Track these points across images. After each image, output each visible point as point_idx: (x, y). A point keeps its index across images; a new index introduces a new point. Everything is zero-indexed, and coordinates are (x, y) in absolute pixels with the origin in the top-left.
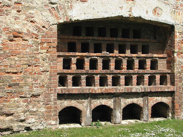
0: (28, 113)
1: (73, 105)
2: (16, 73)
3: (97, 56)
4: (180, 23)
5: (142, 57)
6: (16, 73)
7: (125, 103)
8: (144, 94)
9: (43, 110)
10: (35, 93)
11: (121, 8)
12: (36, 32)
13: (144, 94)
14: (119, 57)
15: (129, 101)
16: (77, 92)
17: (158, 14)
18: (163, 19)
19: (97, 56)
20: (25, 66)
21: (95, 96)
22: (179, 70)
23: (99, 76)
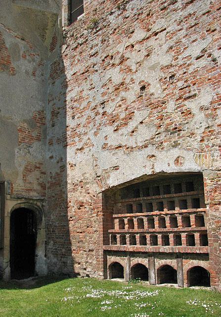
0: (88, 264)
1: (117, 261)
2: (81, 233)
3: (143, 216)
4: (209, 168)
5: (184, 213)
6: (81, 233)
7: (159, 263)
8: (179, 256)
9: (95, 262)
10: (91, 248)
11: (145, 167)
12: (90, 201)
13: (179, 256)
14: (162, 215)
15: (163, 262)
16: (116, 250)
17: (181, 163)
18: (187, 168)
19: (143, 216)
20: (85, 227)
21: (133, 254)
22: (213, 226)
23: (139, 235)
